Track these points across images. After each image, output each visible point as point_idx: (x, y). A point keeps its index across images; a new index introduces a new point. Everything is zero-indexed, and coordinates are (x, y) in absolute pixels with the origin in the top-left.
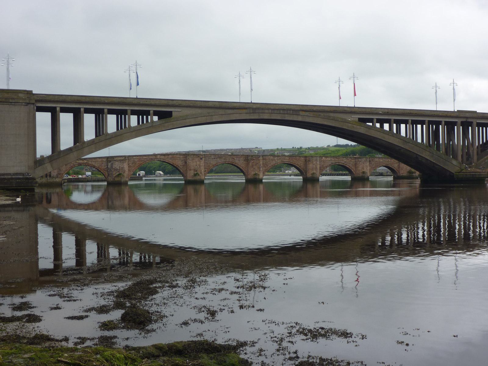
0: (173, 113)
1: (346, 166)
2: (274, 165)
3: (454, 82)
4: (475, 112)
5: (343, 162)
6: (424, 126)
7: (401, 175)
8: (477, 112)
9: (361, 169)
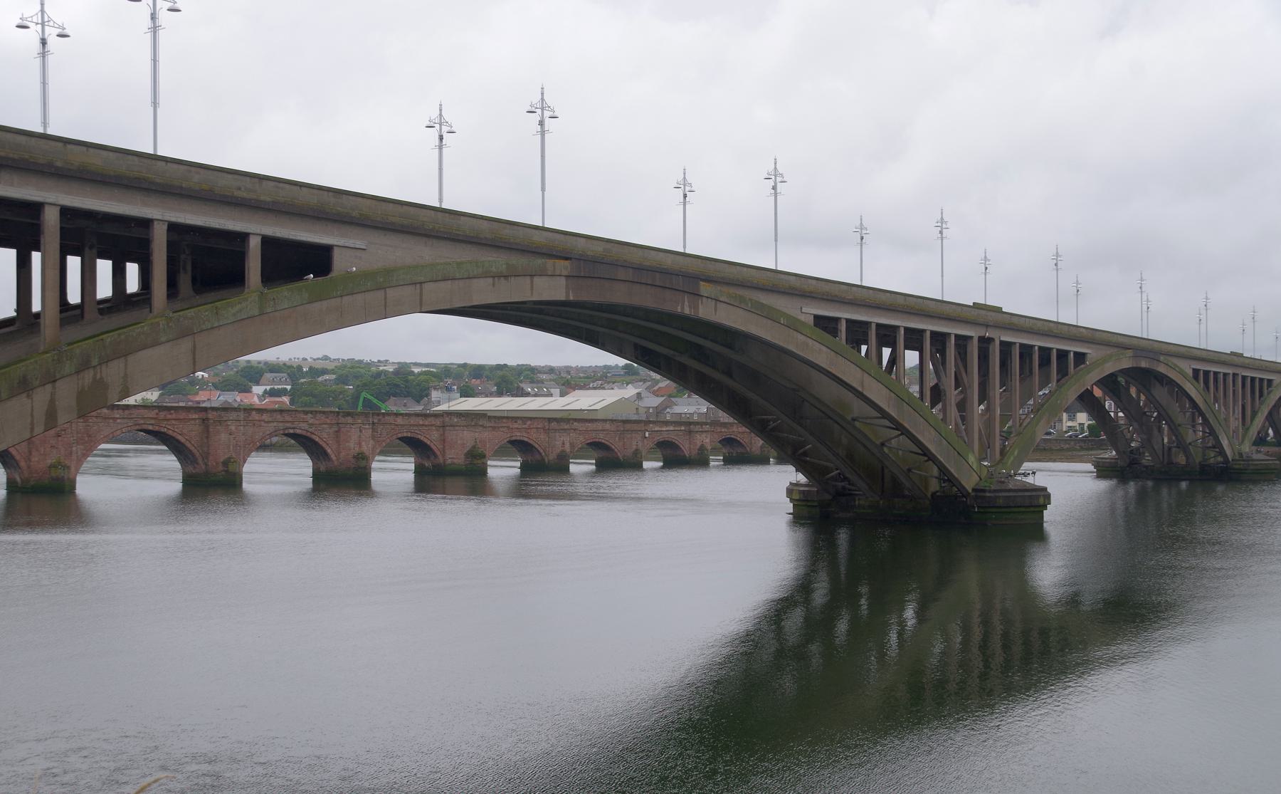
0: (337, 255)
1: (595, 442)
2: (111, 436)
3: (42, 11)
4: (998, 310)
5: (304, 426)
6: (36, 257)
7: (449, 461)
8: (1004, 310)
9: (352, 446)
